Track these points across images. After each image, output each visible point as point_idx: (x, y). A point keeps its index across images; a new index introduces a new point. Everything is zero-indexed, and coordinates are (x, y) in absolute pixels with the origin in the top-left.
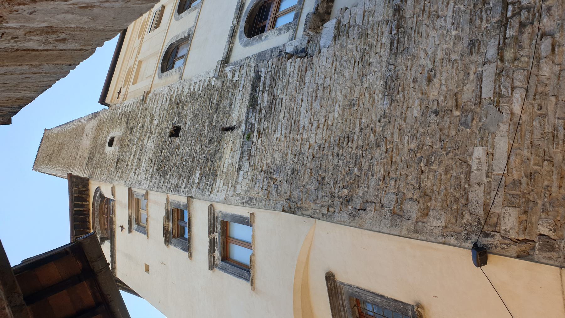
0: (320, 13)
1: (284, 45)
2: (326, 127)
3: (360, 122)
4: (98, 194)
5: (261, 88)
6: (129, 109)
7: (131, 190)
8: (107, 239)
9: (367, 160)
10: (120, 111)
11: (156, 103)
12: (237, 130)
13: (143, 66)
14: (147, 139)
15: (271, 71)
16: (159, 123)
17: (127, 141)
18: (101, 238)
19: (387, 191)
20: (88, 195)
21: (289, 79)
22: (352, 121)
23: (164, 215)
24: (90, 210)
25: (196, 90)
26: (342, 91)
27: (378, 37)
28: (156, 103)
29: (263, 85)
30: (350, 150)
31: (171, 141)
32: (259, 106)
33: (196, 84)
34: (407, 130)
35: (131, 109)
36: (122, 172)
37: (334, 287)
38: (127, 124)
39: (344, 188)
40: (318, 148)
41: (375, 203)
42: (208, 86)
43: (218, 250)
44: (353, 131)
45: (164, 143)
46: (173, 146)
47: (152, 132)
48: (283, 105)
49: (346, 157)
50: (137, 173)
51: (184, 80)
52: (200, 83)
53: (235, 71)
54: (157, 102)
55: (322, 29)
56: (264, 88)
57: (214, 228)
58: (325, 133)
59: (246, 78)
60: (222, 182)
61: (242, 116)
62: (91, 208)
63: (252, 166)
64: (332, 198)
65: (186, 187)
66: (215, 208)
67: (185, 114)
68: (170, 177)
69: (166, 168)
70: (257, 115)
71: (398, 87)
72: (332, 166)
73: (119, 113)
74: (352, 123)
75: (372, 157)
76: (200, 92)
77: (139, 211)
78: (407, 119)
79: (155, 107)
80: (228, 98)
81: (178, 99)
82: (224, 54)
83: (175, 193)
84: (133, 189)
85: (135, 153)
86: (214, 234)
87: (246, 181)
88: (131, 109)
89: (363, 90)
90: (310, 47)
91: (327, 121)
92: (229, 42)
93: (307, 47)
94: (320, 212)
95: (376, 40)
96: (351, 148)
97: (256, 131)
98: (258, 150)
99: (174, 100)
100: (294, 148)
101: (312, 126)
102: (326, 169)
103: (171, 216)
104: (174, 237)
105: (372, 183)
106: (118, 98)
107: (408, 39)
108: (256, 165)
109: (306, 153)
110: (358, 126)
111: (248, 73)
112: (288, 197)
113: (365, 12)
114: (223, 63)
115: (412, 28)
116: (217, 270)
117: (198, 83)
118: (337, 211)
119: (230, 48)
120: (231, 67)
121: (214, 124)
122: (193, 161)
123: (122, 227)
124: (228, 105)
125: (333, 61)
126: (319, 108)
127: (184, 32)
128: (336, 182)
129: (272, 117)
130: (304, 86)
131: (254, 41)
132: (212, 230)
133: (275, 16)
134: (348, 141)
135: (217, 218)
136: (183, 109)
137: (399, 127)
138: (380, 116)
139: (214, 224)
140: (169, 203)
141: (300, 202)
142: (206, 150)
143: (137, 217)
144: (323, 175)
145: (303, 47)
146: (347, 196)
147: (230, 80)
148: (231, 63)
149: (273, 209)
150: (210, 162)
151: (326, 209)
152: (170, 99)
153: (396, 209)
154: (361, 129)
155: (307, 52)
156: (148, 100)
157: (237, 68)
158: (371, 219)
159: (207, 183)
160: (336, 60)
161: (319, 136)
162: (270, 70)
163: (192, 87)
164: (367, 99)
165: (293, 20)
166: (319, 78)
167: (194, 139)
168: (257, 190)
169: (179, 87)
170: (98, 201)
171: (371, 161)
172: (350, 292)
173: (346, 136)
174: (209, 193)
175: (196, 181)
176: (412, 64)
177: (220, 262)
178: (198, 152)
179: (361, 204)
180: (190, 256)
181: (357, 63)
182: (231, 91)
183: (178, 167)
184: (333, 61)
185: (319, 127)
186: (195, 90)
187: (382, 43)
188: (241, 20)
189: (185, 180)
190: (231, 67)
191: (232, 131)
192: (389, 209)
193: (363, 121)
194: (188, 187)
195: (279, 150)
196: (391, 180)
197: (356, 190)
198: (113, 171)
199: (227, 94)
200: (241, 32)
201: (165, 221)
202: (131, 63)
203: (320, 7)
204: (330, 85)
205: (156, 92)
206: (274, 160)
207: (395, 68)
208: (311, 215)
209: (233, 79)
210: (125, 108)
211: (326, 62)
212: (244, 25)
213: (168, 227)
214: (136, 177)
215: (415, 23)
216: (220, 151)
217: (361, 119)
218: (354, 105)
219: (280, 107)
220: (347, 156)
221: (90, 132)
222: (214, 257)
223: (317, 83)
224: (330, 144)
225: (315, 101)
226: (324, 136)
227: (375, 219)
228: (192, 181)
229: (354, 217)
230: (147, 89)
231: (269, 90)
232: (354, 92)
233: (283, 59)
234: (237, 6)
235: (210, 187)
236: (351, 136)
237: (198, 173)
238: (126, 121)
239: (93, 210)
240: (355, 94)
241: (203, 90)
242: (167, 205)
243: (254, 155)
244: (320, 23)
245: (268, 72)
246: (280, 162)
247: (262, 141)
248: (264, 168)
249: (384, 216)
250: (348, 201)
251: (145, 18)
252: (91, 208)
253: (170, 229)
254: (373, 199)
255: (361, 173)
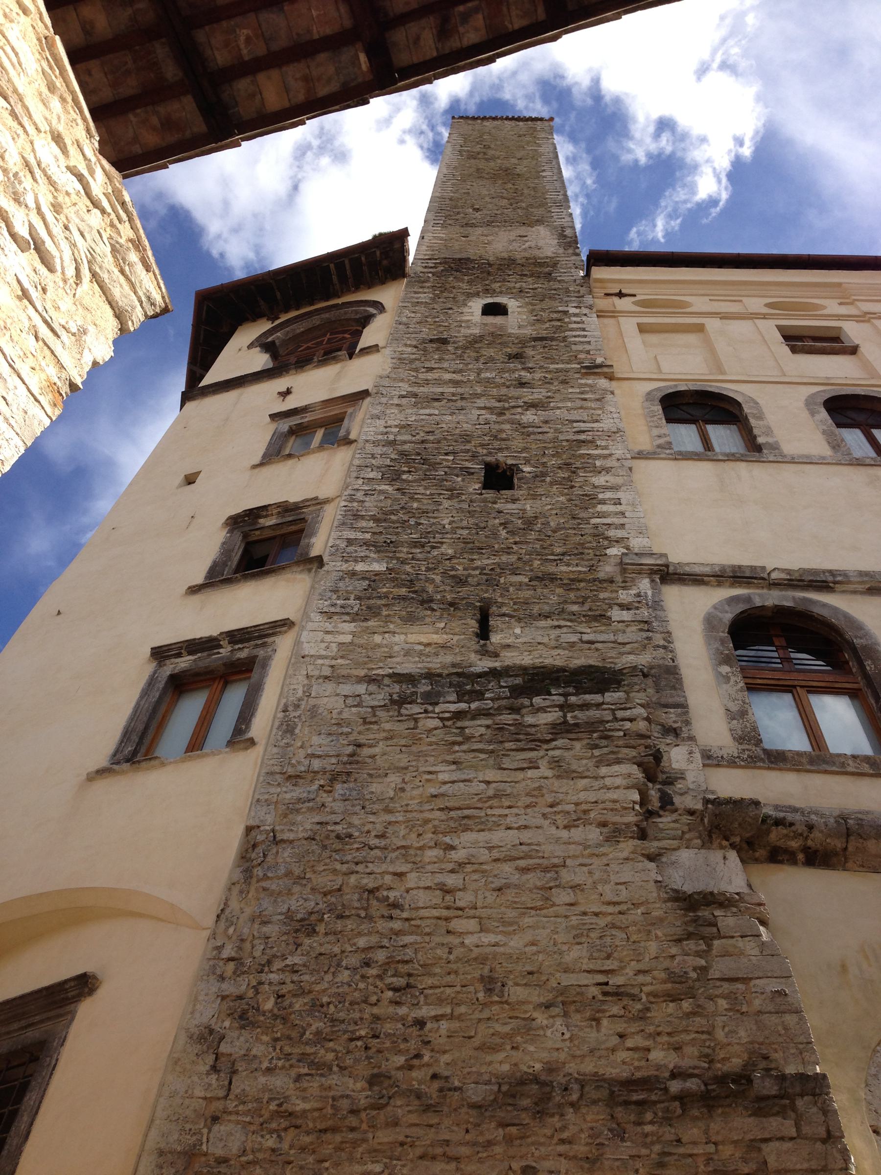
0: (768, 835)
1: (692, 738)
2: (445, 913)
3: (442, 1016)
4: (372, 310)
5: (573, 699)
6: (574, 333)
7: (363, 399)
8: (275, 356)
9: (340, 1055)
10: (572, 311)
11: (579, 403)
12: (477, 647)
13: (692, 338)
14: (488, 405)
15: (616, 719)
16: (524, 427)
17: (491, 352)
18: (273, 342)
19: (252, 1128)
20: (357, 288)
21: (585, 777)
22: (448, 991)
23: (292, 500)
24: (339, 297)
25: (600, 508)
26: (533, 944)
27: (669, 1034)
28: (579, 403)
29: (580, 703)
30: (374, 999)
31: (472, 471)
32: (526, 702)
33: (615, 504)
34: (399, 1167)
35: (573, 339)
36: (412, 361)
37: (67, 999)
38: (535, 339)
39: (279, 997)
40: (392, 900)
41: (226, 1097)
42: (607, 538)
43: (195, 660)
44: (422, 998)
45: (470, 454)
46: (460, 479)
47: (505, 414)
48: (518, 773)
49: (356, 989)
50: (404, 401)
51: (630, 469)
52: (616, 513)
53: (637, 608)
54: (581, 408)
55: (722, 847)
56: (572, 707)
57: (241, 641)
58: (427, 915)
59: (612, 645)
60: (348, 638)
61: (513, 654)
62: (339, 301)
63: (375, 715)
64: (256, 966)
65: (350, 542)
66: (285, 636)
67: (540, 491)
68: (381, 492)
69: (404, 477)
70: (504, 702)
71: (517, 1121)
72: (339, 952)
73: (566, 309)
74: (442, 993)
75: (345, 1068)
76: (594, 521)
77: (321, 427)
78: (428, 1163)
79: (569, 404)
80: (565, 602)
81: (582, 463)
82: (688, 564)
83: (340, 517)
84: (368, 400)
85: (456, 383)
86: (229, 643)
87: (340, 703)
88: (573, 339)
89: (526, 1012)
90: (674, 822)
91: (460, 913)
92: (719, 573)
93: (676, 810)
94: (230, 938)
95: (660, 1029)
96: (378, 1001)
97: (463, 706)
98: (412, 724)
99: (582, 452)
100: (403, 827)
101: (452, 871)
102: (335, 934)
103: (290, 519)
104: (245, 536)
105: (280, 1082)
106: (607, 295)
107: (646, 1135)
108: (375, 727)
109: (384, 867)
110: (433, 1013)
111: (628, 646)
112: (279, 837)
113: (745, 980)
114: (661, 570)
115: (679, 1141)
116: (151, 667)
117: (619, 508)
118: (225, 986)
119: (705, 578)
120: (650, 593)
121: (502, 580)
122: (415, 544)
123: (288, 392)
124: (547, 608)
125: (618, 903)
126: (493, 886)
127: (769, 431)
128: (297, 972)
129: (491, 747)
130: (561, 826)
131: (717, 645)
132: (238, 636)
133: (795, 687)
134: (396, 990)
135: (264, 645)
136: (551, 484)
137: (409, 1139)
138: (447, 1078)
139: (249, 640)
140: (319, 507)
141: (261, 874)
142: (437, 574)
143: (304, 425)
144: (321, 928)
145: (677, 800)
146: (258, 1010)
147: (613, 599)
148: (660, 592)
149: (257, 797)
150: (403, 591)
151: (233, 954)
152: (584, 442)
153: (203, 1159)
154: (420, 1023)
155: (661, 813)
156: (590, 382)
157: (645, 613)
158: (186, 1092)
159: (352, 597)
160: (620, 913)
161: (423, 898)
162: (620, 714)
163: (608, 495)
164: (499, 1029)
165: (765, 751)
166: (577, 870)
167: (469, 534)
168: (312, 743)
169: (614, 457)
170: (357, 312)
171: (335, 1069)
172: (54, 1041)
173: (412, 981)
174: (325, 610)
175: (360, 567)
176: (575, 1157)
177: (168, 673)
178: (435, 553)
179: (231, 1055)
180: (194, 590)
181: (601, 978)
182: (584, 609)
183: (402, 508)
184: (618, 903)
185: (447, 891)
186: (599, 506)
187: (649, 1050)
188: (783, 593)
189: (368, 536)
190: (650, 593)
191: (477, 635)
192: (205, 1140)
193: (444, 1025)
194: (351, 549)
195: (404, 785)
196: (275, 1136)
197: (267, 1034)
198: (420, 336)
199: (578, 598)
200: (748, 599)
201: (278, 505)
202: (700, 304)
203: (785, 831)
204: (554, 905)
205: (609, 397)
206: (379, 776)
207: (572, 1105)
208: (227, 912)
209: (616, 608)
210: (578, 323)
211: (617, 884)
212: (769, 603)
213: (266, 516)
214: (396, 401)
215: (690, 1152)
216: (429, 612)
217: (451, 1017)
218: (490, 990)
219: (515, 765)
220: (358, 992)
221: (527, 244)
222: (179, 655)
223: (564, 866)
224: (398, 933)
225: (517, 869)
226: (423, 913)
227: (187, 1102)
228: (362, 554)
229: (201, 1039)
230: (619, 370)
231: (565, 722)
232: (525, 985)
233: (642, 748)
234: (824, 572)
235: (342, 607)
236: (406, 998)
237: (379, 567)
238: (544, 334)
239: (336, 306)
240: (518, 988)
241: (596, 527)
242: (314, 502)
243: (402, 715)
244: (737, 839)
245: (613, 710)
246: (372, 793)
247: (436, 729)
248: (366, 751)
249: (187, 1129)
250: (243, 1016)
251: (824, 307)
252: (339, 301)
253: (261, 521)
254: (236, 1089)
255: (307, 1044)
